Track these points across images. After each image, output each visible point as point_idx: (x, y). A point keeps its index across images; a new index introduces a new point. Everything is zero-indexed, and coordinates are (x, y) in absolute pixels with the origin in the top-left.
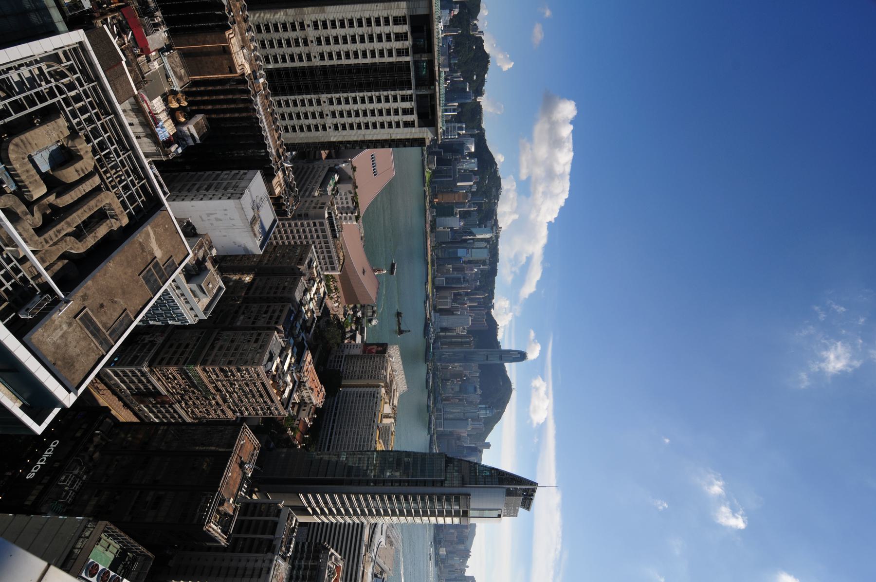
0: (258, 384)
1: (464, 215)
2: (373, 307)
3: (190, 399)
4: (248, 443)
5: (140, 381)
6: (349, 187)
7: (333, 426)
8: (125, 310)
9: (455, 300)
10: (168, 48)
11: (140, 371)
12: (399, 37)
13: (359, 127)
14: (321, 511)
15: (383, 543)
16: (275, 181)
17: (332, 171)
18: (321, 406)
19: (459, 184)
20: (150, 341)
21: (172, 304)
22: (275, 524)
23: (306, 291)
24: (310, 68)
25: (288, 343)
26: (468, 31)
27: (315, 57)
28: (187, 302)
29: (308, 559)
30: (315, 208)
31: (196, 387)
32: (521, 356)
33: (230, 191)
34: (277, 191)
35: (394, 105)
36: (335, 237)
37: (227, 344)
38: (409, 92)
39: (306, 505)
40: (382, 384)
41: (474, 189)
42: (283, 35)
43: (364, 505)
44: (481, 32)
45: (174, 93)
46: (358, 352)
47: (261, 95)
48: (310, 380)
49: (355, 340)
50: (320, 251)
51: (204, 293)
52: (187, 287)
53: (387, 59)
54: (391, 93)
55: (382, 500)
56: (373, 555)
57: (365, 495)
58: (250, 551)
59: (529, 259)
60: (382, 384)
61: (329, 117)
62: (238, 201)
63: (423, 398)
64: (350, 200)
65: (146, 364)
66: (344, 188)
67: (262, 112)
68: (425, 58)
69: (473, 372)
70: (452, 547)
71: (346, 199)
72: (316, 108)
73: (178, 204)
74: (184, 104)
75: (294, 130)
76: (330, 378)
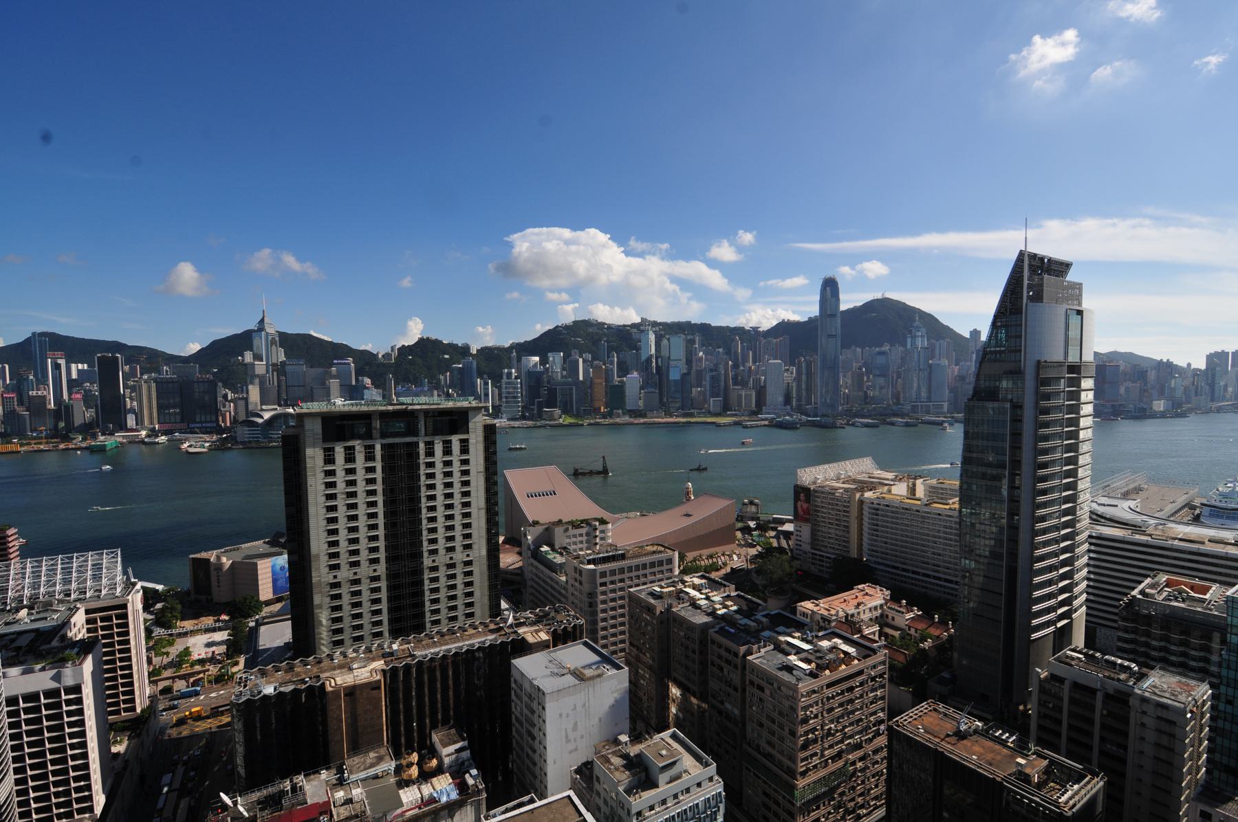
1: (624, 370)
2: (744, 504)
3: (853, 799)
4: (925, 722)
6: (558, 531)
9: (744, 384)
10: (340, 771)
12: (350, 458)
13: (467, 515)
14: (1065, 605)
15: (1132, 504)
16: (531, 639)
17: (536, 554)
18: (888, 592)
19: (581, 378)
22: (1076, 686)
23: (694, 604)
25: (769, 640)
26: (391, 365)
28: (688, 790)
29: (1148, 634)
30: (581, 583)
32: (830, 288)
34: (544, 636)
35: (340, 474)
36: (623, 557)
38: (422, 445)
39: (1052, 629)
40: (858, 495)
44: (392, 348)
45: (398, 770)
46: (806, 530)
47: (414, 648)
48: (843, 605)
50: (643, 580)
51: (674, 763)
52: (664, 789)
54: (423, 470)
55: (1045, 505)
56: (1152, 521)
58: (1125, 735)
59: (675, 280)
60: (858, 495)
61: (454, 556)
62: (547, 698)
66: (560, 538)
67: (437, 650)
68: (377, 424)
69: (854, 356)
70: (1136, 390)
71: (575, 536)
72: (442, 573)
73: (551, 785)
74: (415, 757)
75: (470, 605)
76: (845, 575)
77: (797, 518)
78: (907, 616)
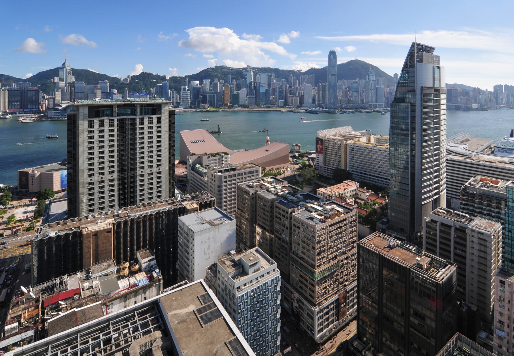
0: (330, 229)
1: (239, 87)
2: (293, 146)
3: (342, 277)
4: (375, 242)
5: (327, 313)
6: (205, 158)
7: (374, 176)
8: (225, 343)
9: (294, 94)
11: (318, 313)
12: (102, 125)
14: (436, 189)
15: (465, 146)
16: (188, 207)
17: (193, 168)
18: (359, 184)
19: (219, 91)
20: (298, 303)
21: (264, 287)
22: (442, 224)
23: (268, 190)
24: (119, 179)
26: (127, 84)
27: (112, 176)
28: (263, 276)
30: (215, 181)
31: (333, 273)
32: (332, 55)
33: (189, 238)
34: (195, 206)
36: (235, 169)
37: (301, 248)
38: (138, 120)
39: (431, 199)
40: (345, 142)
41: (223, 82)
42: (97, 195)
43: (431, 159)
44: (128, 77)
45: (118, 271)
46: (321, 157)
48: (338, 190)
49: (315, 158)
50: (241, 180)
51: (256, 263)
52: (251, 275)
53: (116, 133)
56: (473, 154)
57: (423, 158)
58: (465, 246)
60: (345, 142)
62: (195, 234)
63: (362, 116)
64: (215, 158)
65: (313, 308)
66: (205, 161)
67: (141, 213)
68: (116, 110)
69: (343, 84)
70: (463, 100)
71: (212, 160)
72: (146, 177)
76: (340, 176)
77: (317, 152)
78: (366, 194)
